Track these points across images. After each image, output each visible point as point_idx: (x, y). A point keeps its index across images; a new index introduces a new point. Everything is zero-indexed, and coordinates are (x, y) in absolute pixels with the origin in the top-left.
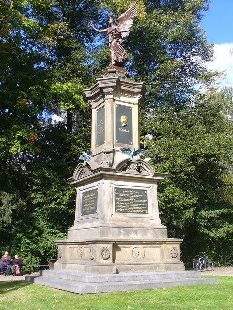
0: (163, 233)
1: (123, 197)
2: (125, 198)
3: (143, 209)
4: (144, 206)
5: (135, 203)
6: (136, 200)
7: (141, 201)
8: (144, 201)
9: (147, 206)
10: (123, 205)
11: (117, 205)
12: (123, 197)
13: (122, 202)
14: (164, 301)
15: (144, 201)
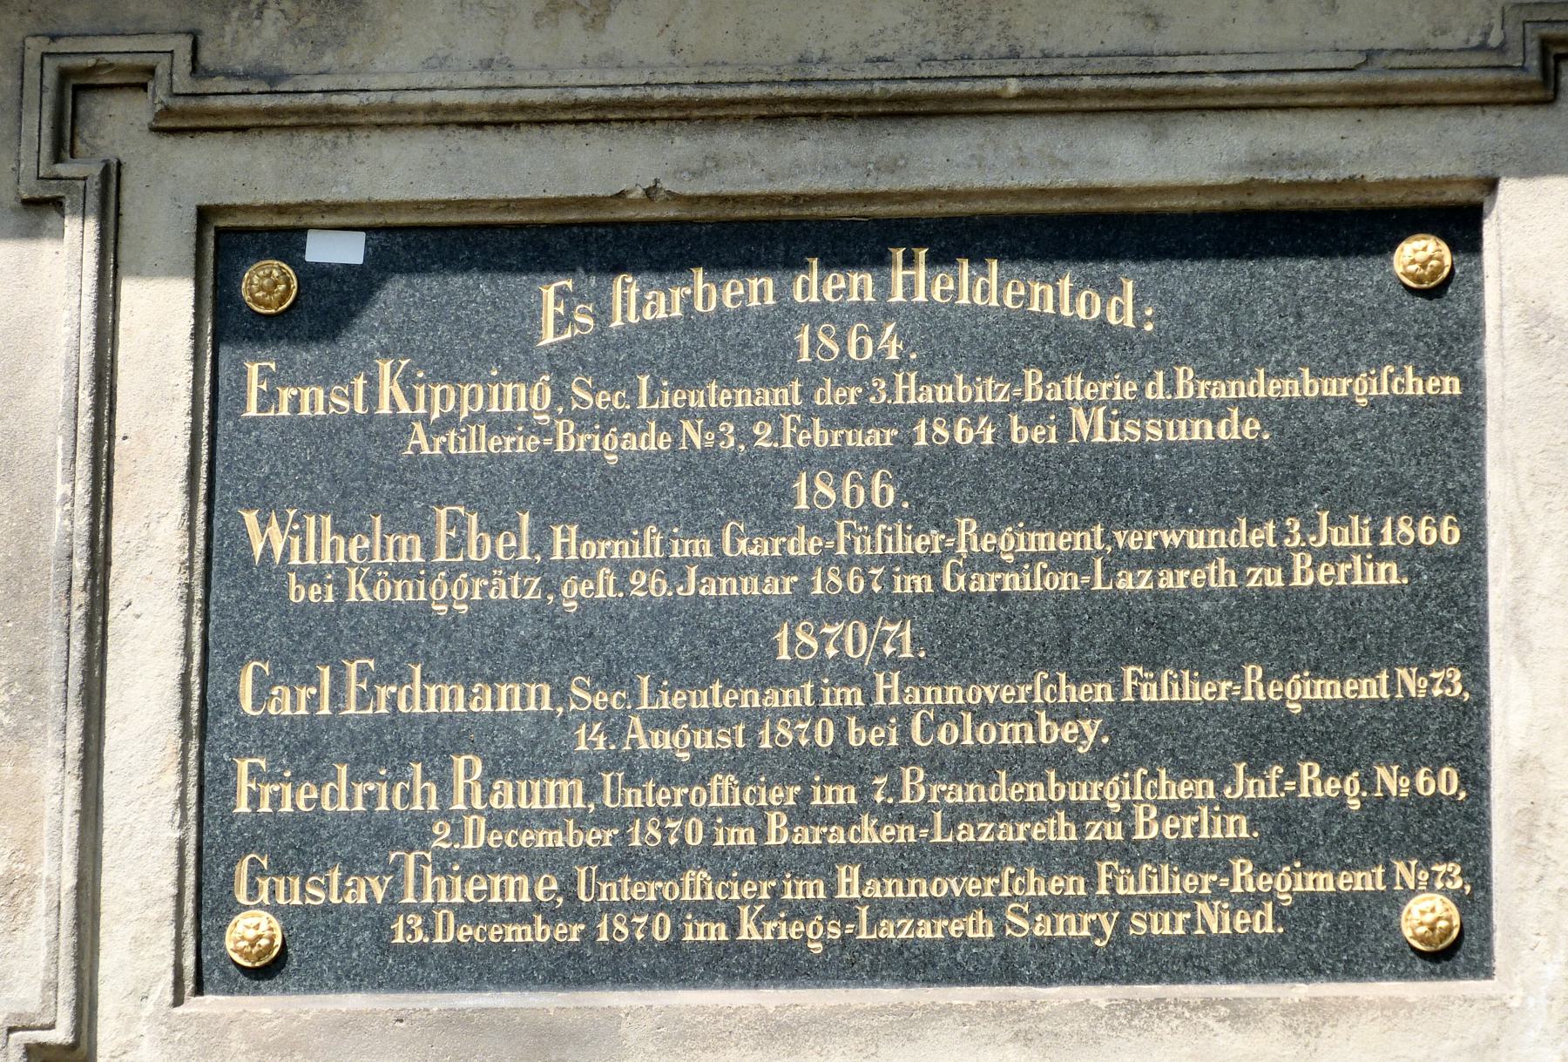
0: (296, 141)
1: (495, 490)
2: (602, 498)
3: (1286, 834)
4: (1338, 739)
5: (970, 637)
6: (1024, 561)
7: (1213, 559)
8: (1345, 555)
9: (1461, 735)
10: (520, 752)
11: (304, 748)
12: (495, 490)
13: (988, 860)
14: (1076, 61)
15: (1345, 555)
